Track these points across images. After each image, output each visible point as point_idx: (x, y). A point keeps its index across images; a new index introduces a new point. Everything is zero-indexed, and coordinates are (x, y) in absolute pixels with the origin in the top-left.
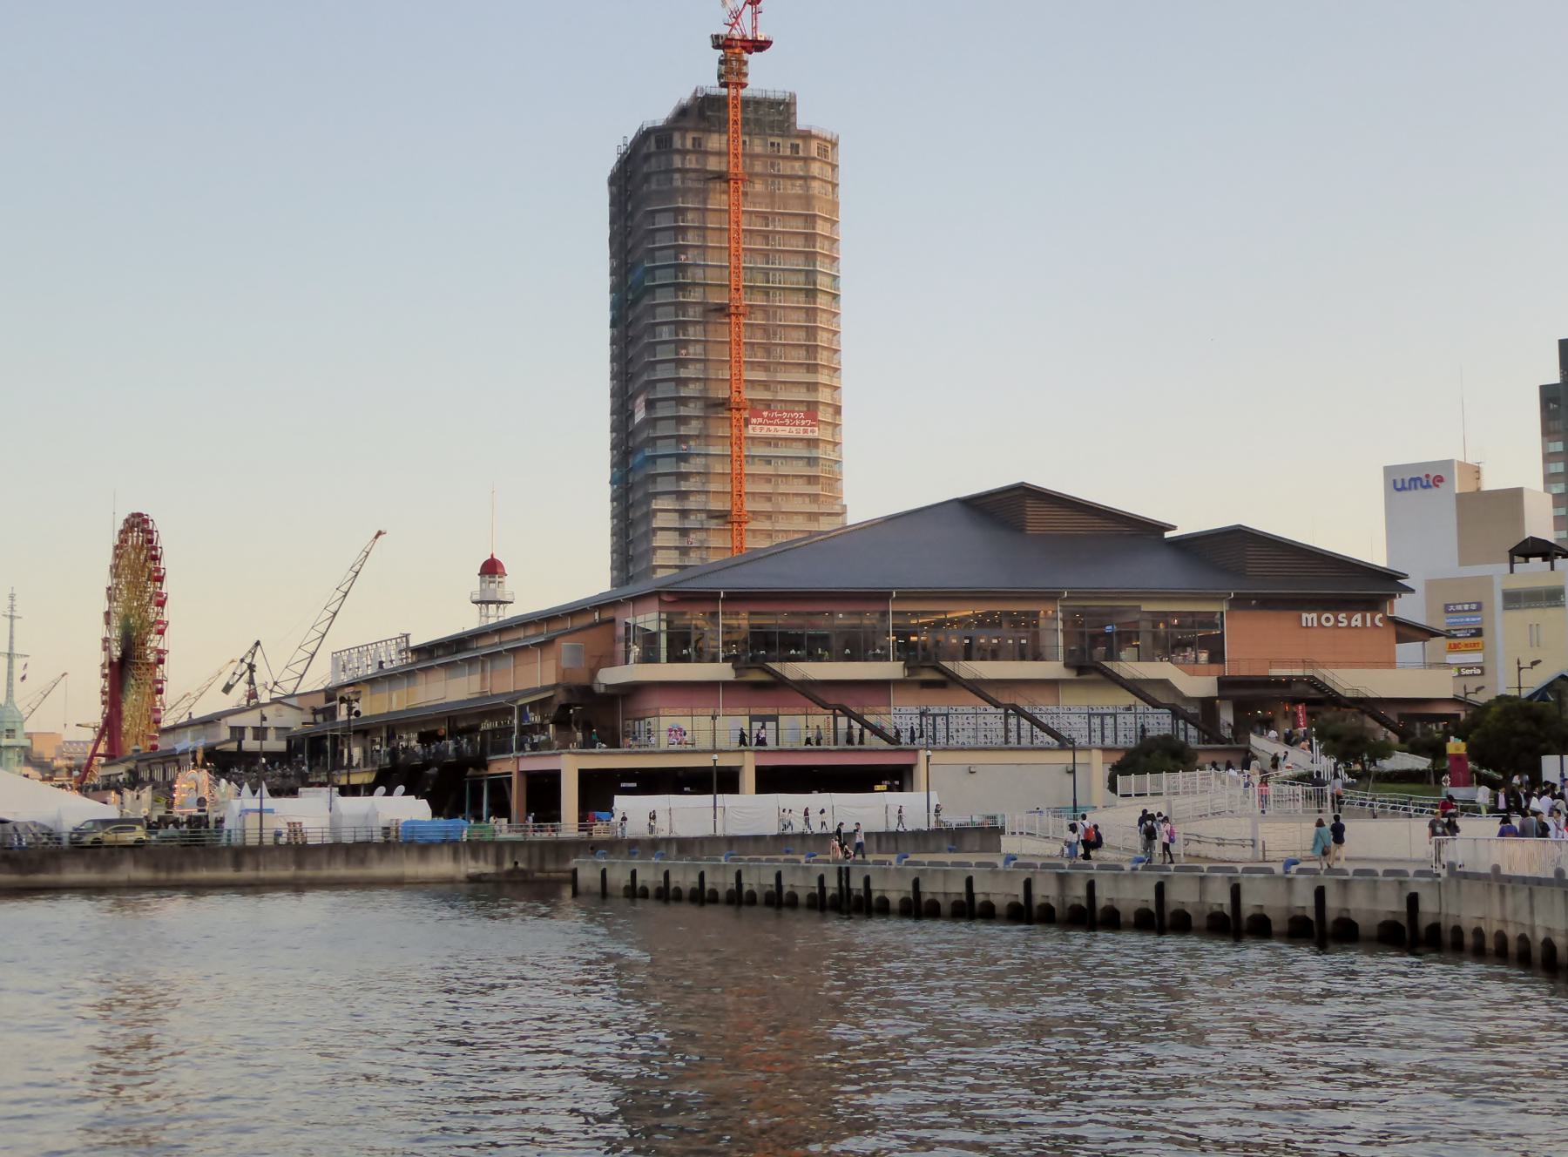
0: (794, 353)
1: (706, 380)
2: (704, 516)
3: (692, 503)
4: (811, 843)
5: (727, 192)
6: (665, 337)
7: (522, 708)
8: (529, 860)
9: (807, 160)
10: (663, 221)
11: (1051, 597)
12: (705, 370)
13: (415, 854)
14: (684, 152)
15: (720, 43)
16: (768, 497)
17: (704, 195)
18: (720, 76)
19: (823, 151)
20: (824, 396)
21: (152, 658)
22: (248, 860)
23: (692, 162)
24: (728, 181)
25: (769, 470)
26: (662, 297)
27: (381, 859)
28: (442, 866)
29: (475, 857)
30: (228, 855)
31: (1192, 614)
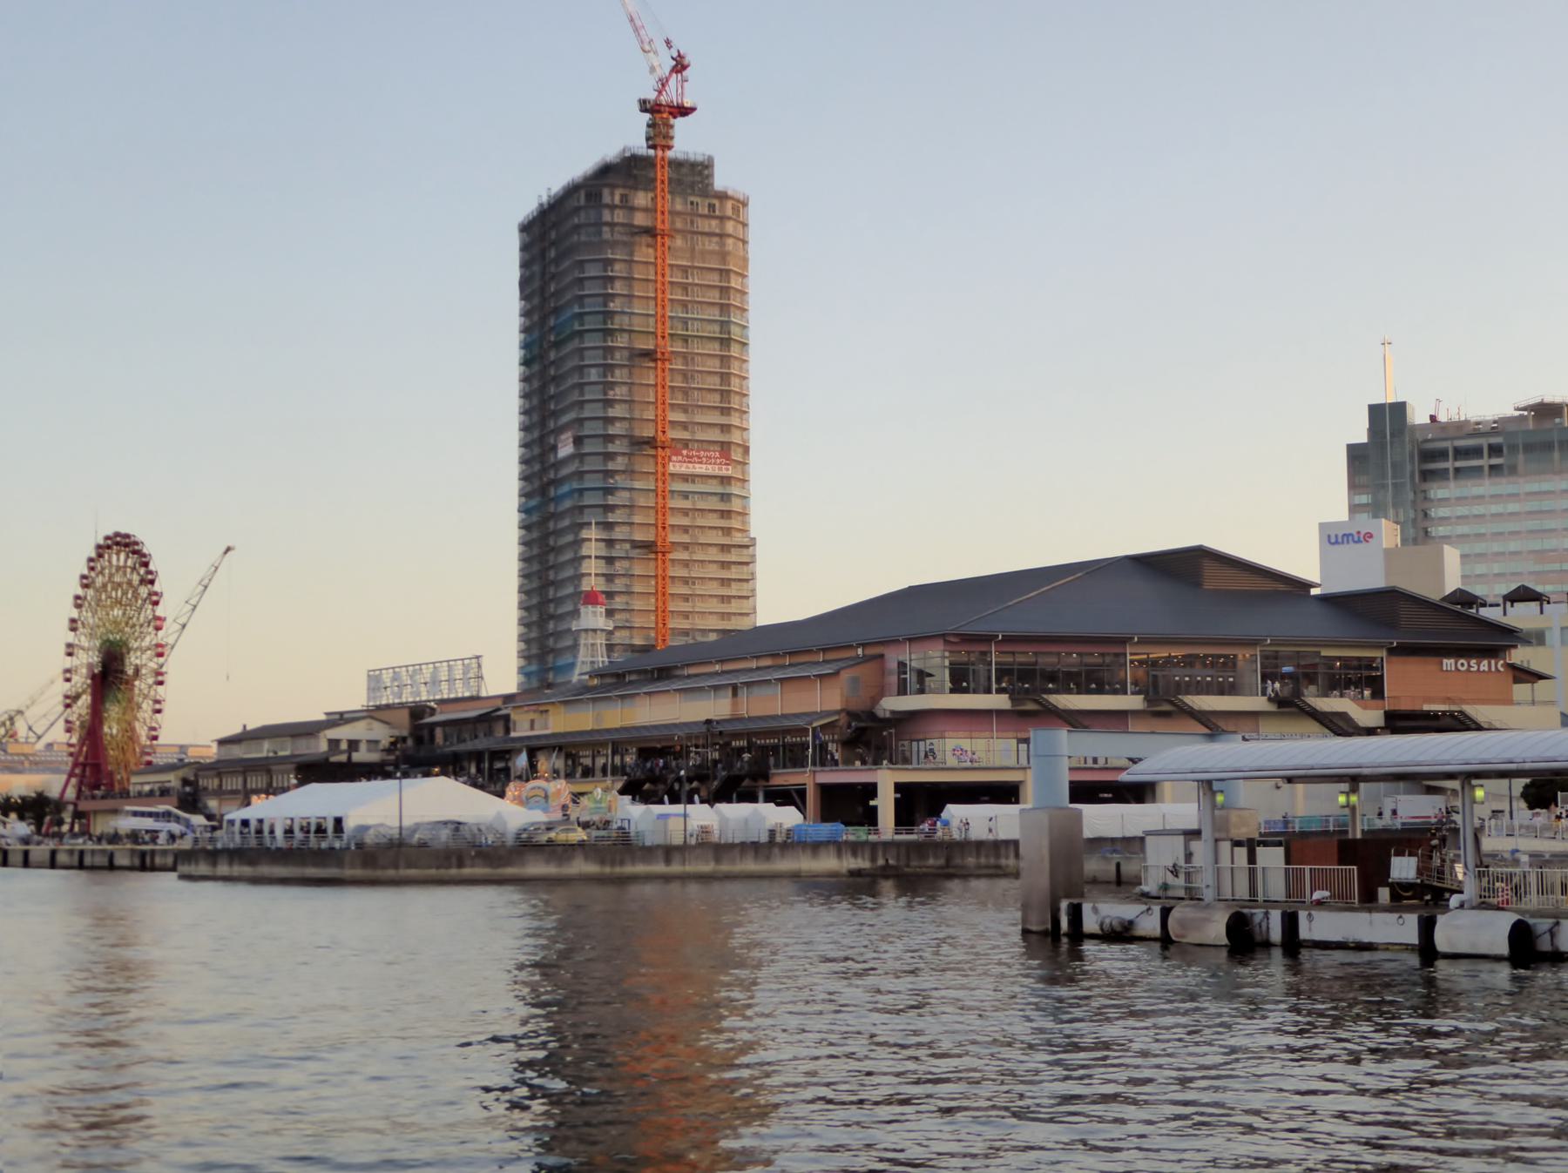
0: (709, 396)
1: (631, 419)
2: (628, 546)
3: (618, 533)
4: (1118, 846)
5: (654, 247)
6: (594, 378)
7: (814, 729)
8: (898, 860)
9: (722, 219)
10: (592, 271)
11: (1252, 643)
12: (631, 410)
13: (809, 852)
14: (612, 207)
15: (645, 106)
16: (685, 529)
17: (630, 247)
18: (648, 139)
19: (736, 210)
20: (736, 437)
21: (130, 672)
22: (677, 857)
23: (620, 216)
24: (655, 236)
25: (687, 504)
26: (590, 341)
27: (783, 856)
28: (829, 863)
29: (855, 854)
30: (660, 853)
31: (1359, 659)
